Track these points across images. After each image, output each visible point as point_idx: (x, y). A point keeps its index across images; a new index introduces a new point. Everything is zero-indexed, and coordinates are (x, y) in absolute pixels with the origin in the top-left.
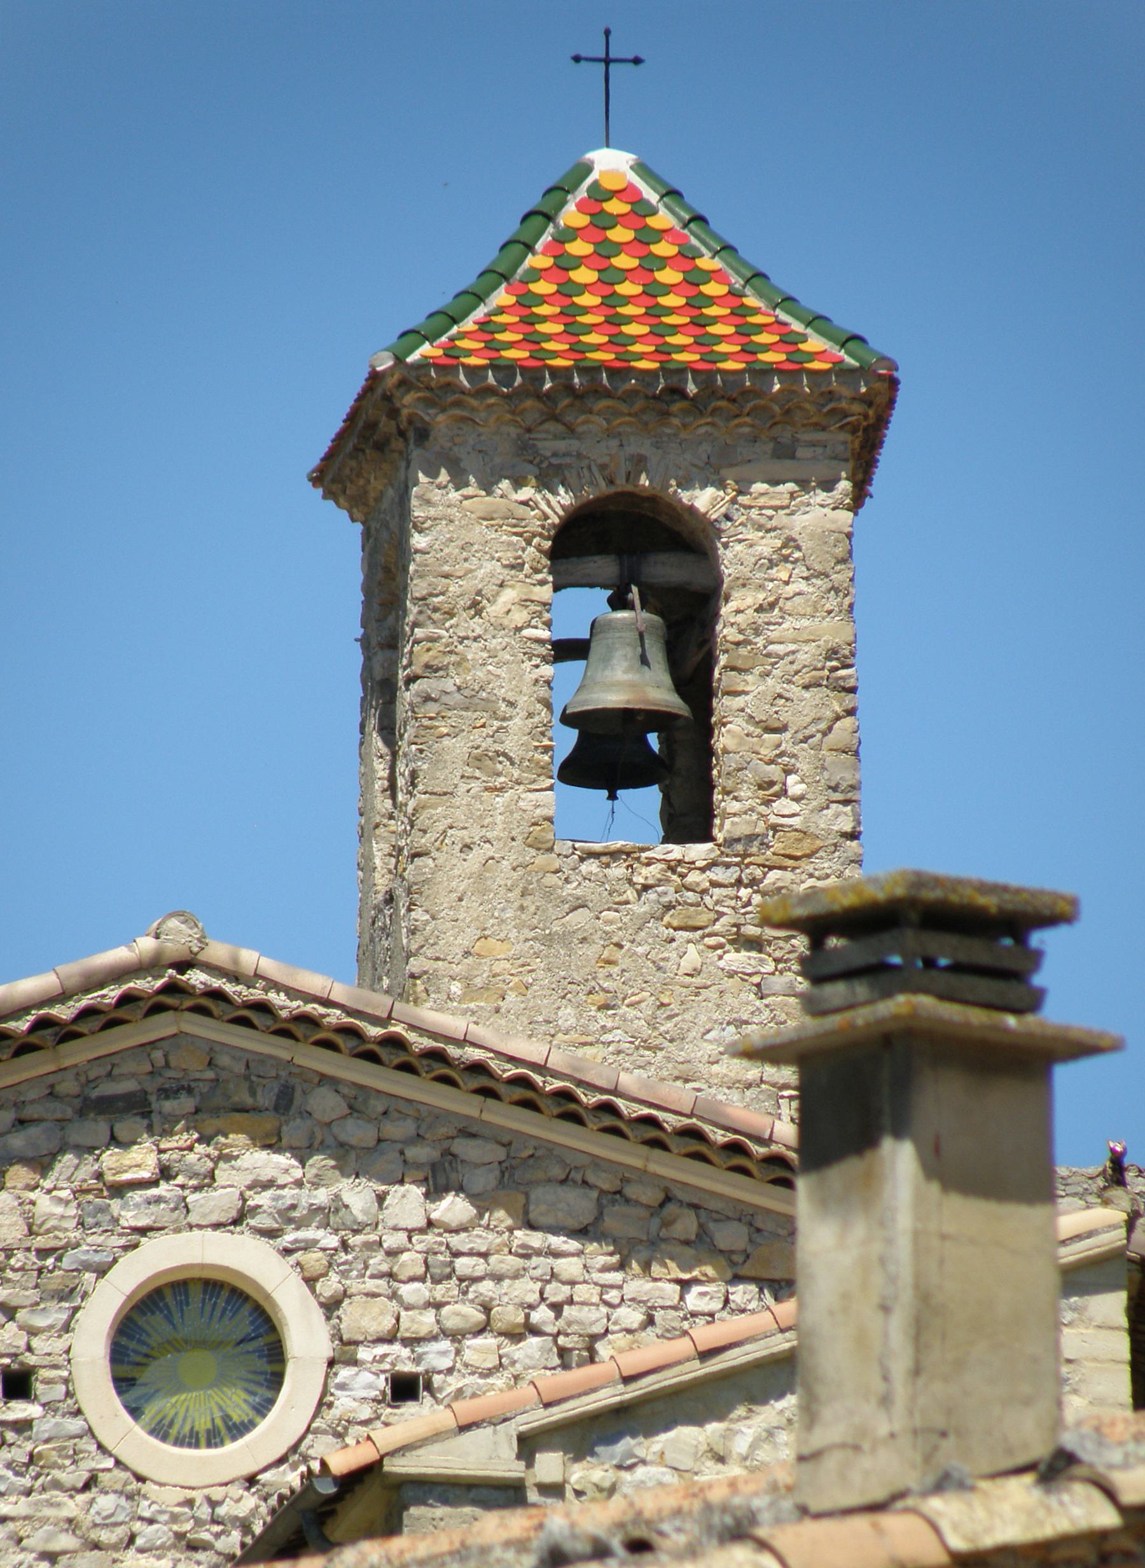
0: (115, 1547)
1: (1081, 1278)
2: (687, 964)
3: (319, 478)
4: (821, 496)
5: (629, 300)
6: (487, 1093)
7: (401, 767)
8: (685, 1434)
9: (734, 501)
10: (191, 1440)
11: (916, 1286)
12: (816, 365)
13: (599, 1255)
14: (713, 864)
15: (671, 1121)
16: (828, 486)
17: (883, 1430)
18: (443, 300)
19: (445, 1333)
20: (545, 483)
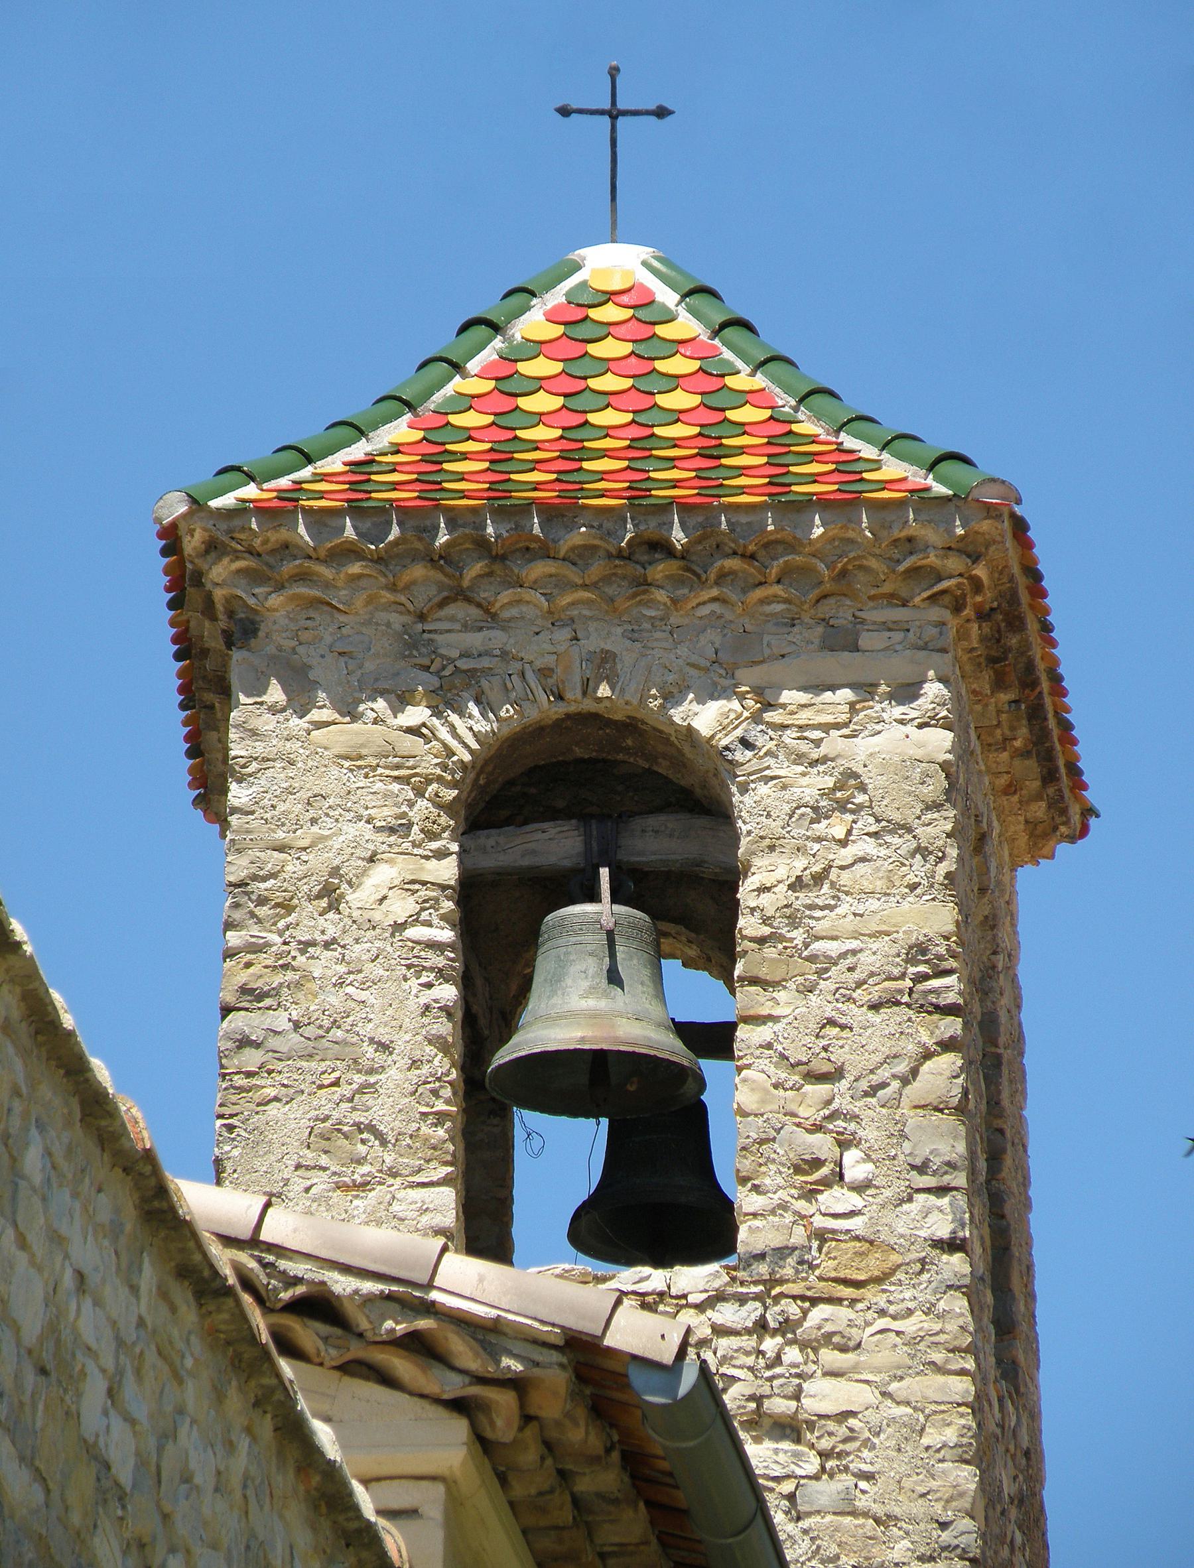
9: (756, 718)
16: (907, 692)
20: (445, 700)
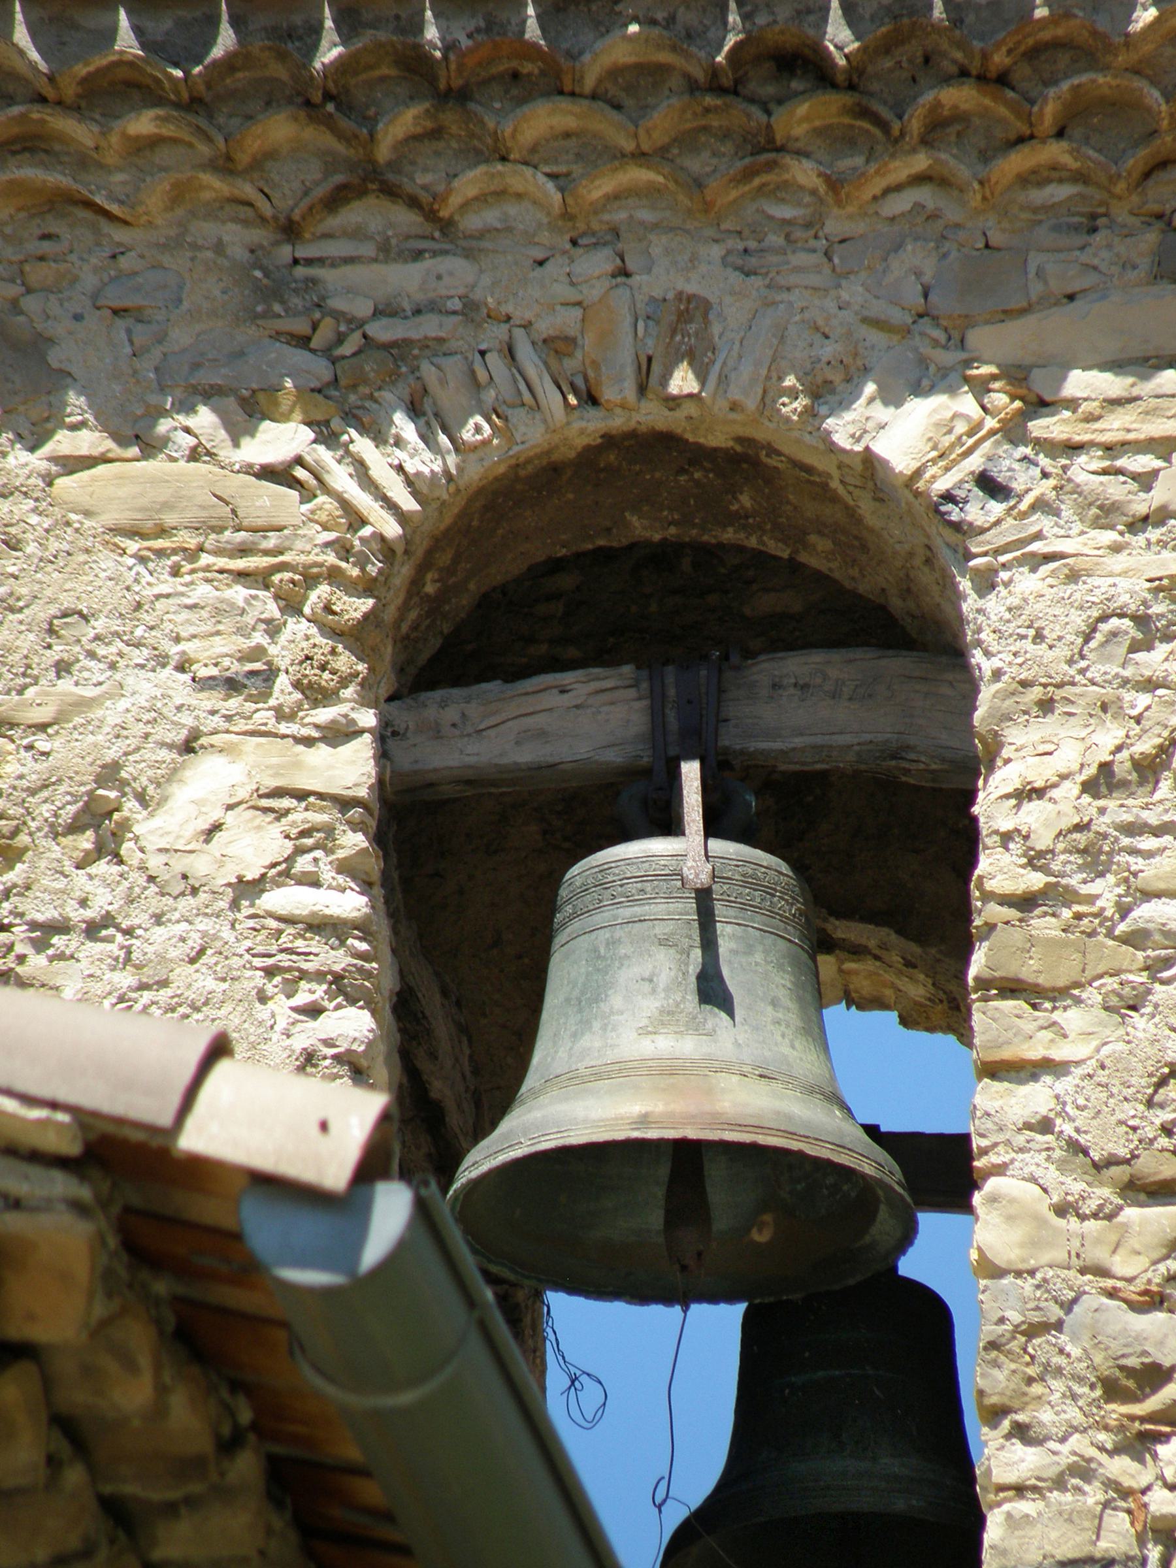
20: (341, 408)
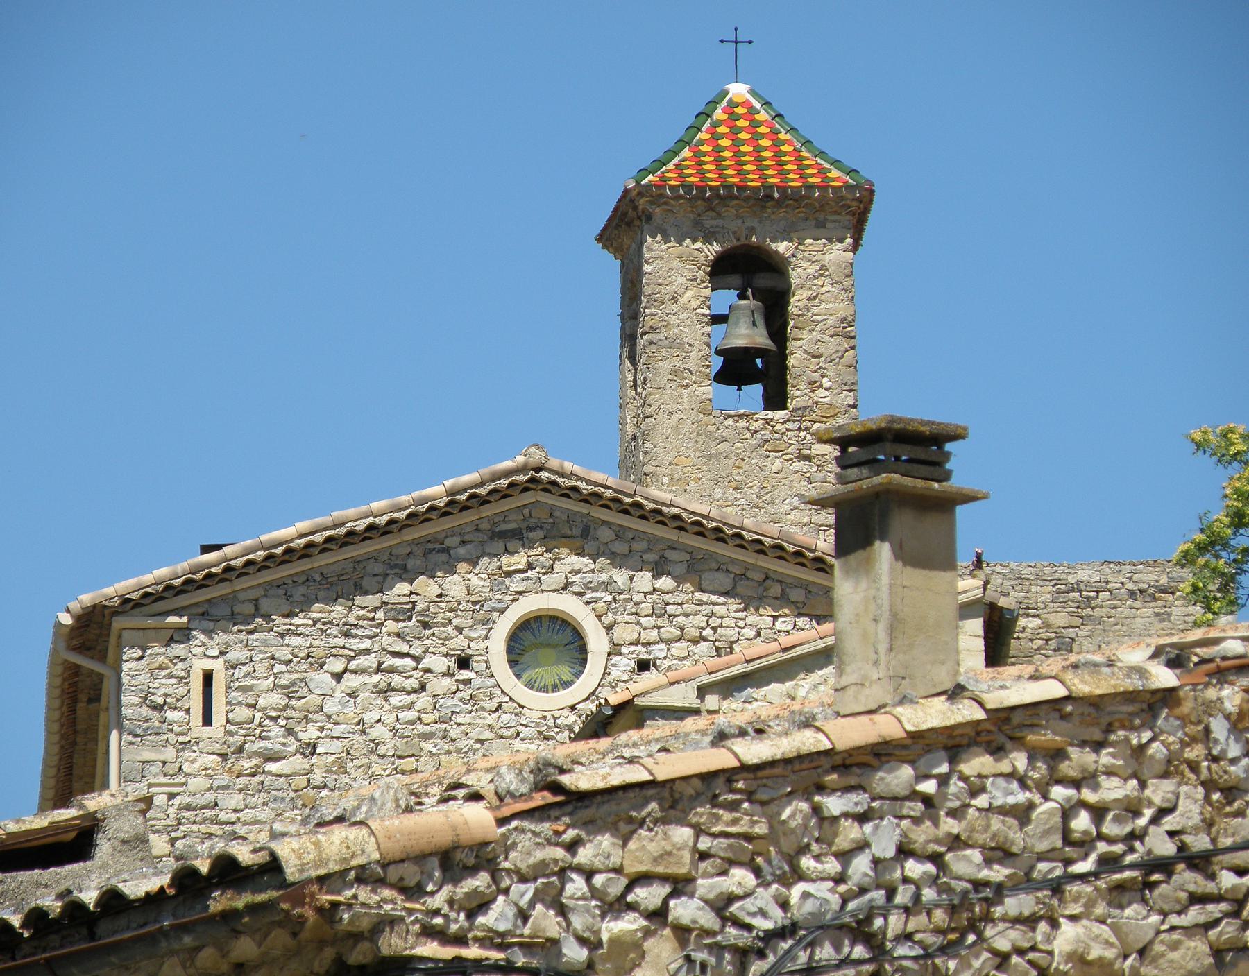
0: (510, 738)
1: (967, 610)
2: (775, 468)
3: (600, 239)
4: (838, 245)
5: (746, 154)
6: (681, 528)
7: (639, 375)
8: (775, 687)
9: (796, 248)
10: (544, 689)
11: (891, 610)
12: (835, 184)
13: (734, 604)
14: (788, 420)
15: (768, 541)
16: (841, 241)
17: (875, 677)
18: (658, 154)
19: (662, 641)
20: (707, 240)
